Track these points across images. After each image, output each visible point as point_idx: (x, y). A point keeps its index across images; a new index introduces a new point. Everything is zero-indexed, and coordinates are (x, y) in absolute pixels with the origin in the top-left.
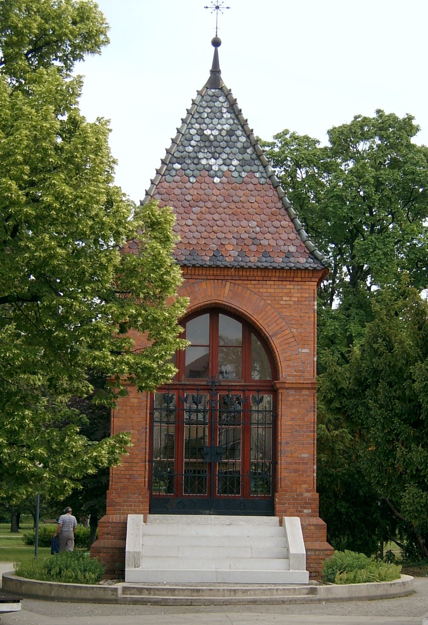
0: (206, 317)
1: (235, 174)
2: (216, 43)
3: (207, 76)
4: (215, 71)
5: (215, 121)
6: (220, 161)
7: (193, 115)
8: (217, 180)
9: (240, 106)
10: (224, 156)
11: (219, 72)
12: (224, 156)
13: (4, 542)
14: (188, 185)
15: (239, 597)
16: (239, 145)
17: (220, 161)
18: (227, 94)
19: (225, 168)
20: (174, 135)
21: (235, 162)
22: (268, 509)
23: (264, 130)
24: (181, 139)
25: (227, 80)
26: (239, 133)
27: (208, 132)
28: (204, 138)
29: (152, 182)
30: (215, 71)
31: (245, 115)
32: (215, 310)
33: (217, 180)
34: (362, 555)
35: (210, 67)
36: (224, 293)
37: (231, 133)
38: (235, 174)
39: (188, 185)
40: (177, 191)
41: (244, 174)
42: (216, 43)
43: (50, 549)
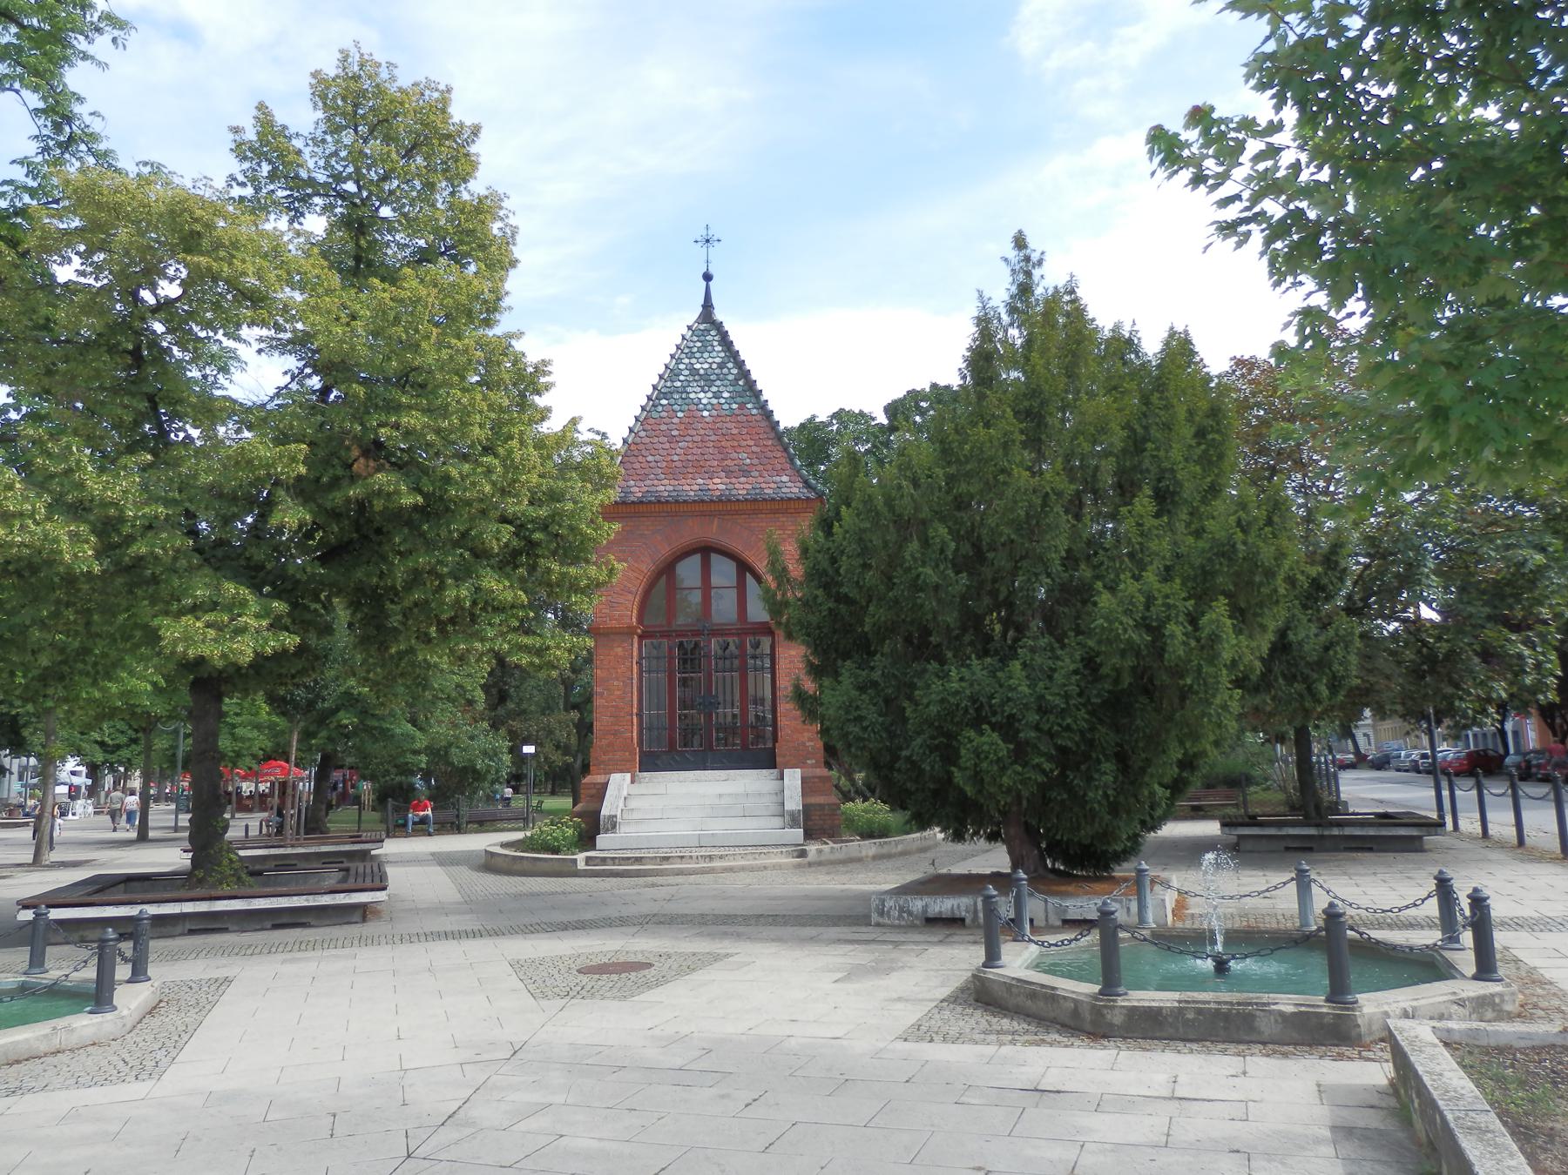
0: (697, 558)
1: (726, 406)
2: (708, 277)
3: (698, 310)
4: (708, 306)
5: (706, 355)
6: (710, 395)
7: (684, 350)
8: (706, 413)
9: (732, 337)
10: (714, 389)
11: (712, 306)
12: (714, 389)
13: (1554, 910)
14: (675, 420)
15: (717, 864)
16: (731, 377)
17: (710, 395)
18: (718, 326)
19: (714, 401)
20: (662, 370)
21: (726, 395)
22: (771, 764)
23: (789, 416)
24: (671, 373)
25: (719, 315)
26: (730, 365)
27: (697, 366)
28: (694, 372)
29: (637, 419)
30: (708, 306)
31: (737, 346)
32: (706, 551)
33: (706, 413)
34: (937, 833)
35: (702, 301)
36: (712, 531)
37: (721, 366)
38: (726, 406)
39: (675, 420)
40: (664, 427)
41: (735, 406)
42: (708, 277)
43: (173, 807)
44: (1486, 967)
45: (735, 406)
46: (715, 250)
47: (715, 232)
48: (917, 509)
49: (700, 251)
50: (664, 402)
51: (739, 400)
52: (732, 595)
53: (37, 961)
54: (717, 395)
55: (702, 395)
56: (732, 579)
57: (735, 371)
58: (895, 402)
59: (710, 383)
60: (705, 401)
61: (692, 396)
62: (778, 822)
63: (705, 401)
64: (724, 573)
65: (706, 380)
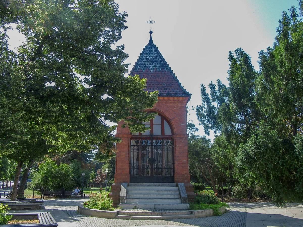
1: (158, 69)
2: (151, 32)
4: (151, 40)
8: (152, 71)
10: (154, 64)
12: (154, 64)
16: (159, 61)
19: (154, 67)
21: (158, 66)
28: (147, 59)
30: (151, 40)
33: (152, 71)
37: (156, 57)
44: (232, 82)
45: (160, 69)
46: (153, 25)
47: (153, 20)
48: (223, 200)
49: (149, 25)
50: (139, 67)
51: (162, 67)
52: (160, 127)
53: (13, 204)
54: (155, 66)
55: (150, 66)
56: (160, 122)
57: (160, 59)
58: (189, 99)
59: (153, 62)
60: (151, 67)
61: (147, 66)
62: (179, 201)
63: (151, 67)
64: (157, 119)
65: (152, 61)
